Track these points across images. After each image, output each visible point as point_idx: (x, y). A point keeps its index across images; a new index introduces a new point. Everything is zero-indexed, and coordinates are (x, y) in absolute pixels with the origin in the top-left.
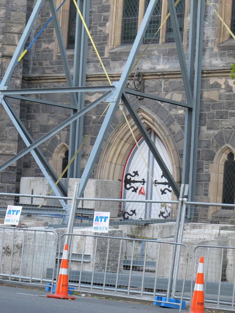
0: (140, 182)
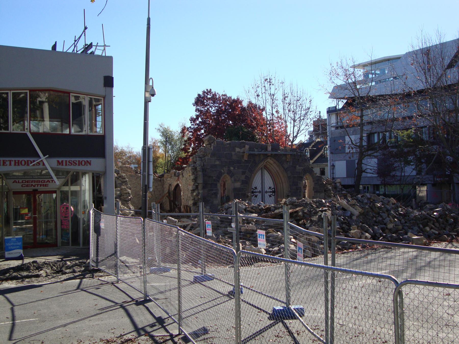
0: (258, 192)
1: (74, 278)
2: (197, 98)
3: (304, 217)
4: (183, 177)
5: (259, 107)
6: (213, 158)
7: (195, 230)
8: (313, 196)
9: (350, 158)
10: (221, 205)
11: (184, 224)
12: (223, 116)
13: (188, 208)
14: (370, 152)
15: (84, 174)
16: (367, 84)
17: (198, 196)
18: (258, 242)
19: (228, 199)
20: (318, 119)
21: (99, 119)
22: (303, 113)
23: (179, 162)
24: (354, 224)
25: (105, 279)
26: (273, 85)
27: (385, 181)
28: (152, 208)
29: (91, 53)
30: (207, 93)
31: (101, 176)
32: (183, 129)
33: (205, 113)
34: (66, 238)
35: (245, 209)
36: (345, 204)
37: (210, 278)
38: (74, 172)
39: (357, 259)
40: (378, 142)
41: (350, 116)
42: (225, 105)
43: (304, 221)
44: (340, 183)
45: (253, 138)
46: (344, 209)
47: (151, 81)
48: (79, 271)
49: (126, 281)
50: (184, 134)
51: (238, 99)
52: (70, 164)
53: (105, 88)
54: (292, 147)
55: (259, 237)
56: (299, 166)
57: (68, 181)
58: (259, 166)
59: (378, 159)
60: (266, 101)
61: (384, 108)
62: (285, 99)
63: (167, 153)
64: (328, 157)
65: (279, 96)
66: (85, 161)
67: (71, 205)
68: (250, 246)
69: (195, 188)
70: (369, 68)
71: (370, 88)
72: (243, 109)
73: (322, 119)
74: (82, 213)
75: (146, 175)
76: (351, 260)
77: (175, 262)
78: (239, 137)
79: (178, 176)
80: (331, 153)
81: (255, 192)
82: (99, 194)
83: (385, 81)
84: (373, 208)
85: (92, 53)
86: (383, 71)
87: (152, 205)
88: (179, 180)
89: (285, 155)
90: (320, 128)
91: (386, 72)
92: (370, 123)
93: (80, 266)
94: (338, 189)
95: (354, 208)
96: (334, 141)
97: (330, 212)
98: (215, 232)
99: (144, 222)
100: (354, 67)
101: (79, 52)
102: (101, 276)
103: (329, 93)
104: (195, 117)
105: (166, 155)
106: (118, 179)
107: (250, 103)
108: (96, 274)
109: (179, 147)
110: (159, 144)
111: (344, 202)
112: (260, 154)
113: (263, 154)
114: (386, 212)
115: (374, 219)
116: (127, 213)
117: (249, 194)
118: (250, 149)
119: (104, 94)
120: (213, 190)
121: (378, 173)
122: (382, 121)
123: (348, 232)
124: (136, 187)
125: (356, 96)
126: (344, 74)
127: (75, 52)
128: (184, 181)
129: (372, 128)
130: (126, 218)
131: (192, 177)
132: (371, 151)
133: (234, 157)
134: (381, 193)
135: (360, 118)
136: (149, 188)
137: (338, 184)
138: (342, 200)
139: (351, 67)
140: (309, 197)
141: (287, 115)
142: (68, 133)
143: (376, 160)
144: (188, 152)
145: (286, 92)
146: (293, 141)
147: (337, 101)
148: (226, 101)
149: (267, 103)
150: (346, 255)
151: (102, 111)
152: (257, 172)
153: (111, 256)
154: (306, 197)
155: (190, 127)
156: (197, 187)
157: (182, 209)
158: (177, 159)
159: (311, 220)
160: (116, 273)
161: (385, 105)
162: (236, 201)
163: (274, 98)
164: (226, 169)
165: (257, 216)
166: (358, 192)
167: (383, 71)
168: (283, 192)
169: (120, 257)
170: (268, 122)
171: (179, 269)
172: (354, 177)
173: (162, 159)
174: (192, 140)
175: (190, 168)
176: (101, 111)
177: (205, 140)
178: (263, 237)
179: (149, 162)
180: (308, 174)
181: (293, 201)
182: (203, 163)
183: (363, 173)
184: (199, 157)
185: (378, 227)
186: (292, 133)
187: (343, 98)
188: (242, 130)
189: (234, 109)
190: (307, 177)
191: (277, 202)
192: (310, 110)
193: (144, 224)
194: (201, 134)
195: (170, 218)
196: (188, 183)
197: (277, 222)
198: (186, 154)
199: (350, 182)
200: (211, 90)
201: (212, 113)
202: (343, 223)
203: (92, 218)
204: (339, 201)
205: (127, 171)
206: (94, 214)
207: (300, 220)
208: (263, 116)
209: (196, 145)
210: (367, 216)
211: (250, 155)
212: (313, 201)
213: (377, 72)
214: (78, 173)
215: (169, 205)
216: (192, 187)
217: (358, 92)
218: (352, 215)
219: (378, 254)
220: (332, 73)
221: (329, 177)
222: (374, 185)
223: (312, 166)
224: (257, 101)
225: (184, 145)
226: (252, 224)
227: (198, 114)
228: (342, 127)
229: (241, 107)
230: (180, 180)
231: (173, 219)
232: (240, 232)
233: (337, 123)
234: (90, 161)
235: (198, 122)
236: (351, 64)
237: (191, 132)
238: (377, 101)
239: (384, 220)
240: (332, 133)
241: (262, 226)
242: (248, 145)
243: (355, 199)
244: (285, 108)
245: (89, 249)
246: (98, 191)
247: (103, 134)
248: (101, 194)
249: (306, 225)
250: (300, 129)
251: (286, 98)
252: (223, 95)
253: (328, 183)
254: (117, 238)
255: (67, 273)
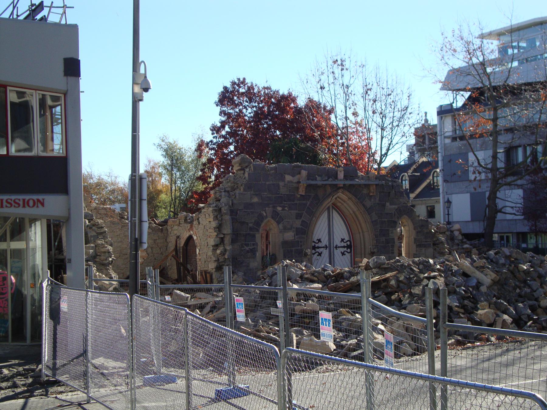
0: (324, 247)
1: (15, 397)
2: (222, 92)
3: (398, 290)
4: (199, 223)
5: (325, 108)
6: (249, 193)
7: (218, 312)
8: (415, 252)
9: (475, 189)
10: (263, 269)
11: (200, 302)
12: (265, 122)
13: (208, 275)
14: (509, 179)
15: (33, 220)
16: (504, 65)
17: (224, 255)
18: (321, 331)
19: (274, 260)
20: (423, 125)
21: (58, 129)
22: (398, 115)
23: (194, 198)
24: (482, 299)
25: (68, 397)
26: (347, 69)
27: (536, 226)
28: (147, 277)
29: (42, 19)
30: (238, 85)
31: (61, 223)
32: (199, 144)
33: (235, 118)
34: (3, 329)
35: (301, 277)
36: (467, 266)
37: (245, 393)
38: (16, 219)
39: (489, 359)
40: (525, 161)
41: (476, 119)
42: (269, 105)
43: (398, 295)
44: (459, 230)
45: (315, 159)
46: (465, 275)
47: (142, 66)
48: (24, 385)
49: (101, 400)
50: (201, 153)
51: (290, 95)
52: (9, 205)
53: (65, 78)
54: (378, 173)
55: (322, 323)
56: (391, 204)
57: (5, 233)
58: (324, 205)
59: (524, 189)
60: (335, 96)
61: (533, 104)
62: (367, 93)
63: (173, 185)
64: (441, 188)
65: (357, 89)
66: (34, 200)
67: (12, 272)
68: (310, 338)
69: (219, 242)
70: (506, 39)
71: (509, 71)
72: (298, 111)
73: (429, 125)
74: (29, 286)
75: (137, 221)
76: (479, 361)
77: (182, 365)
78: (291, 157)
79: (191, 223)
80: (445, 181)
81: (318, 248)
82: (60, 254)
83: (535, 58)
84: (514, 272)
85: (44, 19)
86: (531, 43)
87: (147, 272)
88: (192, 230)
89: (367, 186)
90: (427, 141)
91: (538, 44)
92: (510, 130)
93: (24, 375)
94: (456, 241)
95: (482, 272)
96: (450, 161)
97: (442, 279)
98: (252, 314)
99: (131, 301)
100: (482, 37)
101: (22, 18)
102: (61, 393)
103: (440, 82)
104: (219, 125)
105: (171, 188)
106: (91, 228)
107: (311, 100)
108: (51, 390)
109: (194, 175)
110: (160, 170)
111: (466, 263)
112: (326, 185)
113: (330, 185)
114: (537, 279)
115: (518, 291)
116: (105, 286)
117: (309, 251)
118: (310, 176)
119: (63, 87)
120: (249, 244)
121: (523, 214)
122: (530, 127)
123: (473, 313)
124: (121, 242)
125: (485, 86)
126: (465, 49)
127: (15, 17)
128: (201, 232)
129: (513, 138)
130: (102, 295)
131: (214, 224)
132: (512, 177)
133: (283, 191)
134: (531, 246)
135: (492, 122)
136: (141, 243)
137: (456, 233)
138: (462, 259)
139: (477, 38)
140: (408, 255)
141: (370, 120)
142: (5, 153)
143: (520, 192)
144: (209, 183)
145: (368, 81)
146: (381, 162)
147: (455, 95)
148: (270, 97)
149: (337, 100)
150: (471, 352)
151: (61, 115)
152: (321, 214)
153: (77, 358)
154: (403, 255)
155: (211, 141)
156: (222, 240)
157: (199, 277)
158: (190, 194)
159: (411, 293)
160: (87, 387)
161: (535, 100)
162: (285, 263)
163: (349, 91)
164: (269, 210)
165: (322, 289)
166: (491, 245)
167: (531, 43)
168: (364, 246)
169: (93, 359)
170: (339, 132)
171: (188, 379)
172: (484, 221)
173: (166, 194)
174: (215, 163)
175: (211, 209)
176: (60, 117)
177: (235, 163)
178: (329, 323)
179: (141, 200)
180: (405, 216)
181: (380, 261)
182: (232, 200)
183: (499, 214)
184: (225, 191)
185: (524, 305)
186: (379, 148)
187: (464, 90)
188: (296, 146)
189: (283, 111)
190: (404, 221)
191: (354, 263)
192: (409, 110)
193: (131, 304)
194: (229, 152)
195: (178, 292)
196: (207, 233)
197: (350, 297)
198: (204, 186)
199: (477, 228)
200: (244, 79)
201: (246, 118)
202: (464, 298)
203: (46, 295)
204: (458, 261)
205: (106, 215)
206: (49, 288)
207: (392, 293)
208: (332, 122)
209: (222, 170)
210: (505, 287)
211: (309, 186)
212: (414, 262)
213: (521, 44)
214: (22, 220)
215: (176, 271)
216: (215, 240)
217: (489, 79)
218: (479, 284)
219: (526, 350)
220: (444, 48)
221: (442, 222)
222: (518, 234)
223: (414, 203)
224: (320, 96)
225: (202, 170)
226: (314, 302)
227: (224, 119)
228: (462, 138)
229: (295, 107)
230: (194, 229)
231: (183, 294)
232: (292, 315)
233: (455, 131)
234: (43, 199)
235: (223, 133)
236: (477, 33)
237: (213, 149)
238: (521, 94)
239: (534, 293)
240: (445, 147)
241: (329, 304)
242: (305, 170)
243: (485, 258)
244: (367, 108)
245: (40, 346)
246: (56, 250)
247: (65, 155)
248: (63, 255)
249: (402, 301)
250: (391, 142)
251: (369, 92)
252: (264, 88)
253: (440, 230)
254: (88, 327)
255: (3, 389)
